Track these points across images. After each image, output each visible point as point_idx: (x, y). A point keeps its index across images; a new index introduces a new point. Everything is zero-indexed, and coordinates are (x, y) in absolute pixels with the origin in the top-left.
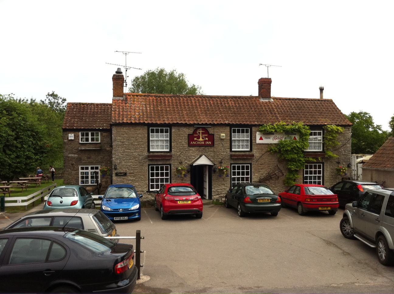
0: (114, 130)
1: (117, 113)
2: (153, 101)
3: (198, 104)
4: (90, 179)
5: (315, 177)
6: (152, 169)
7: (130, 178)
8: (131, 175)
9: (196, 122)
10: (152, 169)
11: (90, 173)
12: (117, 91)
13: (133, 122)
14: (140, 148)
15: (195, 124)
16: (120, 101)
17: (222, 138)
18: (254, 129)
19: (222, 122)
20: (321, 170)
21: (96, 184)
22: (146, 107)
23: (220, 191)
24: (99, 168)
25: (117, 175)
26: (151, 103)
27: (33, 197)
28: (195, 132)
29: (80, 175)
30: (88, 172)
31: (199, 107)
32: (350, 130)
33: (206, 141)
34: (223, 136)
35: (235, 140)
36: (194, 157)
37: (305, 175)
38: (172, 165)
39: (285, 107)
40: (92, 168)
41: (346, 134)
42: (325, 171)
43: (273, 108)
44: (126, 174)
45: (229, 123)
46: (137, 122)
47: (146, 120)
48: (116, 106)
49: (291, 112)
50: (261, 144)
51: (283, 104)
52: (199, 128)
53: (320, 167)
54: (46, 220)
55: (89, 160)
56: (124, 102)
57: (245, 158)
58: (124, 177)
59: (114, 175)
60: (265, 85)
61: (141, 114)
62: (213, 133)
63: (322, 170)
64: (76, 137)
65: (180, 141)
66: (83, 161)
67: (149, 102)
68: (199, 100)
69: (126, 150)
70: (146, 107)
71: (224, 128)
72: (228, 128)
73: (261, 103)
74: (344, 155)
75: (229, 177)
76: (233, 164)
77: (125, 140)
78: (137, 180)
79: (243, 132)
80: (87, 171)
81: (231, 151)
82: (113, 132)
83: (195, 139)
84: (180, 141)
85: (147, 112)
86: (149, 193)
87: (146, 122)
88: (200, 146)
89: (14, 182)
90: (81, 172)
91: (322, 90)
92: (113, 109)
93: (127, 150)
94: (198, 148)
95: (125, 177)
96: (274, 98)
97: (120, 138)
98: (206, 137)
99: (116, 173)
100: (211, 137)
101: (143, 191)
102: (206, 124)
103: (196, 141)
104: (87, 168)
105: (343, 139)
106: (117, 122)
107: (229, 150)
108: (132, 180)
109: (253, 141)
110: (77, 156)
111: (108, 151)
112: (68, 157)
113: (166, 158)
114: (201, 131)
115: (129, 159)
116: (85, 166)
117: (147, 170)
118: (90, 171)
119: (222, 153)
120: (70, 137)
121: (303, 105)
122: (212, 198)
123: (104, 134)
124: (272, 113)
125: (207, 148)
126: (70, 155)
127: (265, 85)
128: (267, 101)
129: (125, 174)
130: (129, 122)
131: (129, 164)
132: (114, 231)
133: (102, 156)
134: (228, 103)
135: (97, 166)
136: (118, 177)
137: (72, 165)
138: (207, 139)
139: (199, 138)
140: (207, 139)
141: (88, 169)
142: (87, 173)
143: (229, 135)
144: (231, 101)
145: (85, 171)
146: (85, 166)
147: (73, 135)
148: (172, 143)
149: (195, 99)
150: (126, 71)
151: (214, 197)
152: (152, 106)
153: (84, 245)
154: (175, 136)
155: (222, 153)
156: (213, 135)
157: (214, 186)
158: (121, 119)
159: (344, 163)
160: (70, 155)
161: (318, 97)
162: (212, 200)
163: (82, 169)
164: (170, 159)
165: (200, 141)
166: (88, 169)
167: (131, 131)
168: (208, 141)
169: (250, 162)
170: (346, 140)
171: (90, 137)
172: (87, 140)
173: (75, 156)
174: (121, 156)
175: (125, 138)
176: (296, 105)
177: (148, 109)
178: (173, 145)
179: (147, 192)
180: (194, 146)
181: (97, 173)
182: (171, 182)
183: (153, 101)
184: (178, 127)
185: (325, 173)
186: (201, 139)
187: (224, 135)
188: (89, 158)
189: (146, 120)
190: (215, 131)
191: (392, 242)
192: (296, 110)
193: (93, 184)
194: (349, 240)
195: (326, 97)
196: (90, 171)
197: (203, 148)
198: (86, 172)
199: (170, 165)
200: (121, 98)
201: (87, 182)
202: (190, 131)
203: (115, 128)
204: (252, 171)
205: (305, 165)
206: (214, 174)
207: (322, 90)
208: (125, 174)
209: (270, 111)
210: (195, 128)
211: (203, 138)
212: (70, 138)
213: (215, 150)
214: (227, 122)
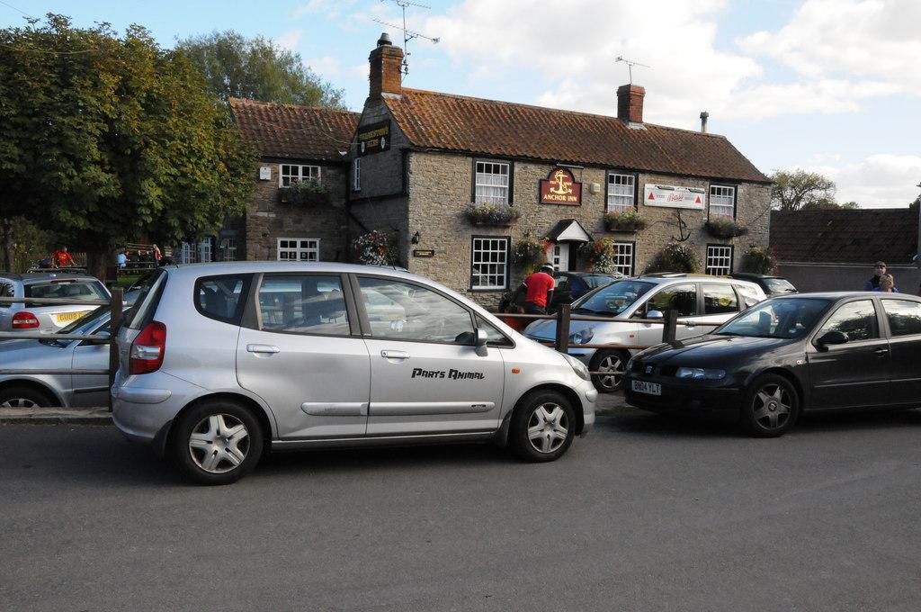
6: (478, 247)
10: (478, 247)
24: (318, 244)
25: (415, 254)
30: (295, 253)
35: (481, 187)
37: (474, 263)
52: (559, 169)
54: (899, 304)
55: (299, 226)
58: (427, 260)
60: (629, 99)
64: (275, 174)
66: (287, 227)
69: (433, 204)
76: (477, 237)
79: (496, 171)
80: (292, 250)
89: (823, 265)
91: (704, 117)
94: (556, 207)
95: (431, 260)
96: (646, 125)
102: (571, 162)
103: (553, 193)
104: (293, 245)
110: (274, 216)
111: (335, 208)
112: (257, 218)
116: (289, 240)
125: (570, 208)
126: (260, 214)
127: (629, 99)
132: (632, 351)
135: (293, 240)
137: (264, 235)
138: (570, 191)
139: (557, 187)
141: (295, 247)
146: (289, 240)
147: (269, 170)
156: (581, 184)
160: (260, 214)
163: (284, 244)
166: (295, 247)
168: (573, 195)
173: (271, 216)
179: (468, 291)
180: (549, 203)
186: (561, 191)
191: (651, 413)
193: (505, 278)
194: (233, 486)
195: (711, 129)
197: (563, 207)
198: (290, 253)
199: (509, 239)
207: (704, 117)
211: (564, 190)
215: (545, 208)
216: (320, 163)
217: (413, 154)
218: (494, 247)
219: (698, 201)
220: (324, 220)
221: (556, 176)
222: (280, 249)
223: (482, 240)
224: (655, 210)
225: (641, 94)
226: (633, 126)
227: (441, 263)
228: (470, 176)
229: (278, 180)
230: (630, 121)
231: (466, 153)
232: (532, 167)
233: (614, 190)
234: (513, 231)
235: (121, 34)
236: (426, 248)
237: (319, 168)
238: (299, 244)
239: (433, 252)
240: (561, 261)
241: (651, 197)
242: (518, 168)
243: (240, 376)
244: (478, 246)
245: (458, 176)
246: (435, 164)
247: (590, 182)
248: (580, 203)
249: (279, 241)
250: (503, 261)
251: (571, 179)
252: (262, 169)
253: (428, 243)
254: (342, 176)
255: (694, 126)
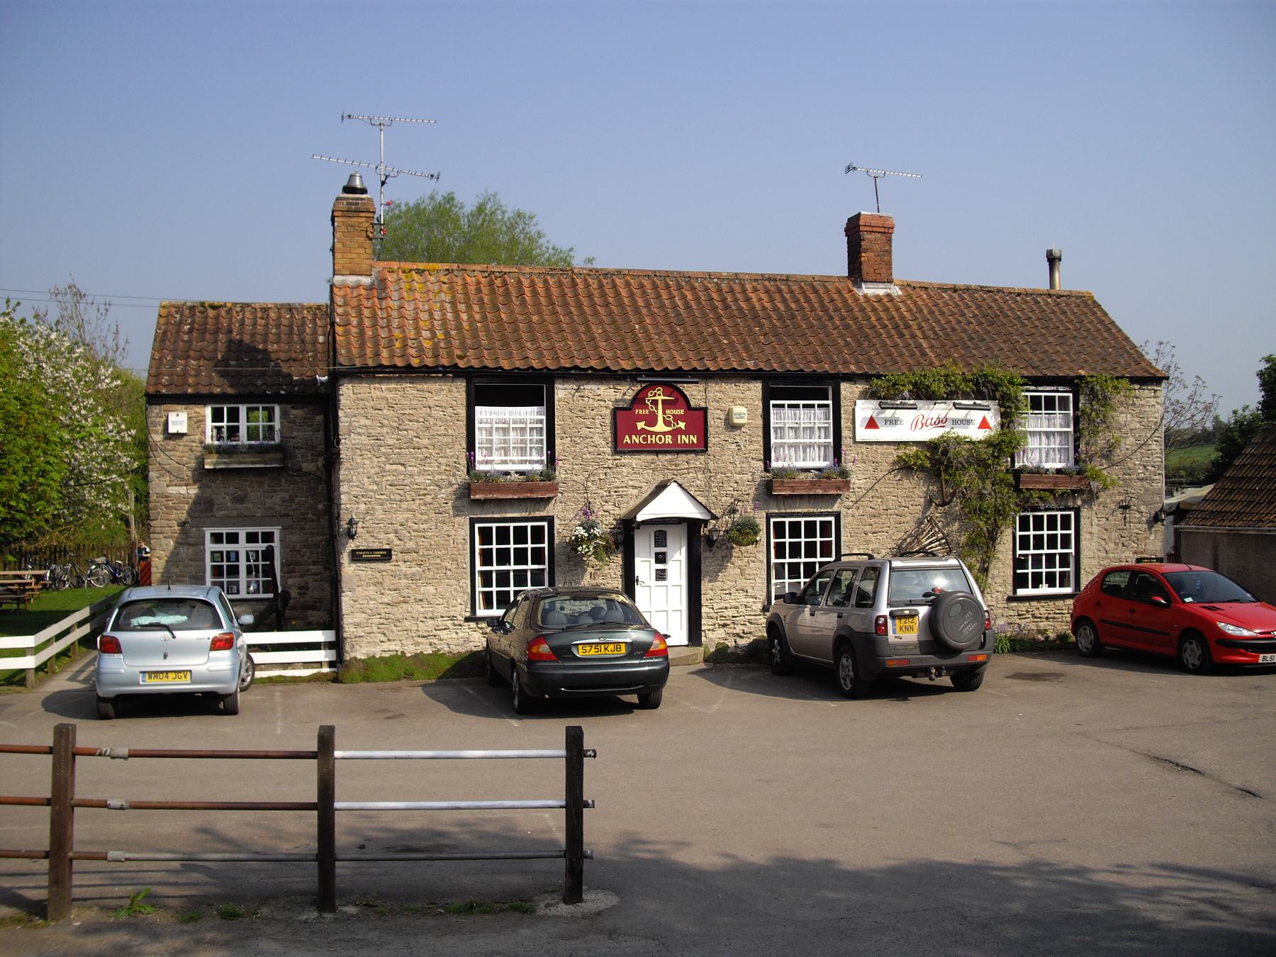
0: (347, 392)
1: (354, 330)
2: (479, 291)
3: (641, 302)
4: (243, 577)
5: (1050, 560)
6: (1024, 527)
7: (403, 567)
8: (407, 557)
9: (640, 364)
11: (242, 557)
12: (349, 255)
13: (415, 362)
14: (441, 460)
15: (638, 369)
16: (363, 292)
17: (736, 421)
18: (845, 388)
19: (735, 365)
20: (777, 557)
21: (271, 595)
22: (456, 312)
23: (726, 613)
25: (356, 556)
26: (472, 297)
27: (59, 637)
28: (638, 400)
29: (209, 564)
30: (237, 553)
31: (644, 311)
32: (1158, 394)
33: (679, 431)
34: (740, 416)
36: (635, 492)
37: (1019, 552)
38: (557, 522)
39: (942, 313)
40: (252, 538)
41: (1147, 409)
42: (1084, 537)
43: (902, 318)
44: (390, 556)
45: (761, 370)
46: (429, 362)
47: (461, 358)
48: (349, 309)
49: (965, 331)
50: (871, 443)
51: (936, 305)
52: (653, 385)
53: (1066, 526)
56: (375, 293)
57: (820, 492)
58: (380, 566)
59: (345, 558)
60: (863, 242)
61: (440, 335)
62: (703, 405)
63: (1072, 532)
64: (196, 422)
65: (585, 432)
66: (220, 509)
67: (466, 294)
68: (642, 286)
69: (388, 467)
70: (456, 312)
71: (743, 386)
72: (756, 388)
73: (862, 300)
74: (1142, 480)
75: (1170, 494)
77: (385, 430)
78: (429, 575)
80: (232, 547)
81: (767, 468)
82: (344, 401)
83: (640, 425)
84: (585, 432)
85: (459, 328)
86: (473, 625)
87: (462, 364)
88: (657, 450)
90: (213, 553)
92: (338, 320)
93: (394, 467)
94: (650, 457)
95: (387, 566)
97: (368, 422)
98: (677, 418)
99: (353, 551)
100: (698, 419)
101: (452, 618)
102: (679, 372)
104: (233, 538)
105: (1138, 426)
106: (358, 363)
107: (760, 465)
108: (412, 577)
109: (845, 433)
113: (534, 496)
114: (663, 397)
115: (398, 497)
116: (224, 531)
117: (468, 539)
118: (242, 547)
119: (738, 477)
120: (175, 423)
121: (1001, 309)
122: (703, 639)
123: (294, 412)
124: (901, 335)
125: (683, 457)
126: (173, 490)
128: (881, 292)
129: (387, 556)
130: (399, 362)
131: (401, 517)
133: (287, 491)
134: (748, 300)
136: (362, 565)
138: (682, 425)
139: (652, 420)
140: (682, 425)
141: (237, 542)
142: (233, 555)
143: (760, 411)
144: (755, 290)
145: (225, 547)
146: (260, 530)
148: (558, 441)
149: (628, 284)
150: (383, 183)
151: (710, 634)
152: (476, 308)
153: (1174, 874)
154: (568, 412)
155: (738, 477)
156: (705, 410)
157: (709, 597)
158: (369, 352)
159: (1143, 508)
160: (173, 490)
161: (1045, 286)
162: (701, 649)
163: (217, 538)
164: (549, 499)
165: (656, 434)
166: (237, 542)
167: (407, 393)
169: (835, 508)
170: (1146, 428)
171: (243, 424)
172: (233, 432)
174: (371, 487)
175: (385, 422)
176: (979, 307)
177: (464, 316)
178: (558, 448)
179: (467, 620)
180: (635, 450)
181: (268, 554)
182: (552, 583)
183: (479, 291)
184: (577, 380)
185: (1083, 544)
186: (660, 427)
187: (743, 410)
188: (240, 500)
189: (461, 358)
190: (710, 395)
192: (980, 324)
195: (1067, 281)
196: (242, 547)
197: (668, 457)
198: (228, 553)
199: (550, 520)
200: (366, 280)
201: (235, 588)
202: (626, 392)
203: (350, 386)
204: (843, 538)
205: (1021, 518)
206: (708, 554)
207: (1053, 260)
208: (387, 556)
209: (896, 327)
210: (638, 387)
211: (667, 423)
212: (172, 430)
213: (711, 465)
214: (750, 364)
215: (626, 459)
216: (280, 400)
217: (346, 380)
218: (1038, 526)
219: (984, 424)
220: (285, 495)
221: (650, 397)
222: (210, 547)
223: (803, 520)
224: (880, 449)
225: (887, 231)
226: (869, 290)
227: (409, 571)
228: (463, 412)
229: (204, 433)
230: (863, 281)
231: (453, 372)
232: (591, 389)
233: (786, 417)
234: (559, 506)
235: (468, 202)
236: (376, 546)
237: (277, 409)
238: (242, 537)
239: (389, 551)
240: (670, 574)
241: (872, 424)
242: (562, 392)
243: (555, 826)
244: (486, 535)
245: (438, 413)
246: (389, 395)
247: (725, 406)
248: (706, 446)
249: (208, 532)
250: (482, 573)
251: (681, 399)
252: (172, 417)
253: (382, 536)
254: (319, 418)
255: (1037, 280)
